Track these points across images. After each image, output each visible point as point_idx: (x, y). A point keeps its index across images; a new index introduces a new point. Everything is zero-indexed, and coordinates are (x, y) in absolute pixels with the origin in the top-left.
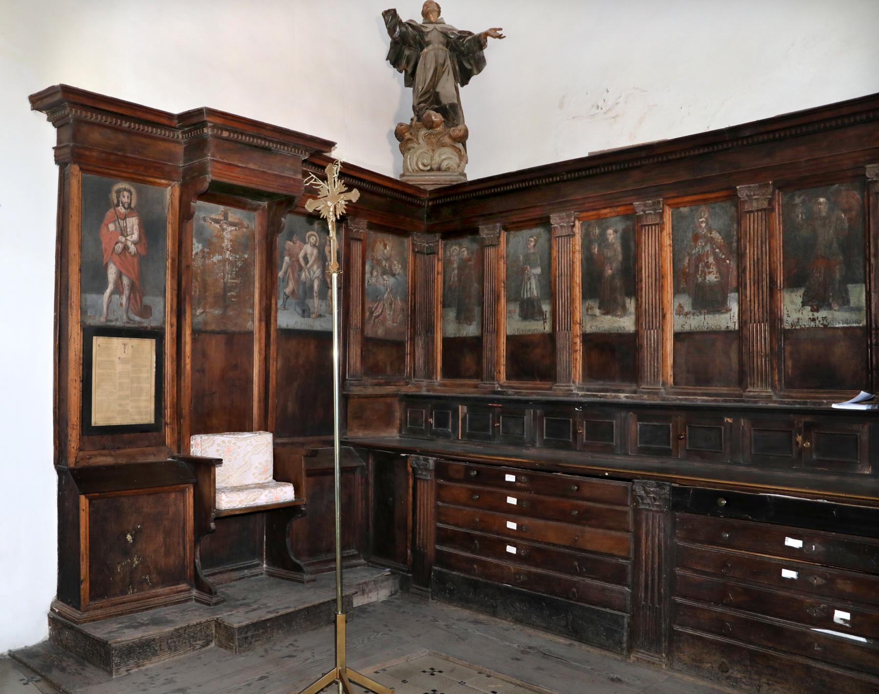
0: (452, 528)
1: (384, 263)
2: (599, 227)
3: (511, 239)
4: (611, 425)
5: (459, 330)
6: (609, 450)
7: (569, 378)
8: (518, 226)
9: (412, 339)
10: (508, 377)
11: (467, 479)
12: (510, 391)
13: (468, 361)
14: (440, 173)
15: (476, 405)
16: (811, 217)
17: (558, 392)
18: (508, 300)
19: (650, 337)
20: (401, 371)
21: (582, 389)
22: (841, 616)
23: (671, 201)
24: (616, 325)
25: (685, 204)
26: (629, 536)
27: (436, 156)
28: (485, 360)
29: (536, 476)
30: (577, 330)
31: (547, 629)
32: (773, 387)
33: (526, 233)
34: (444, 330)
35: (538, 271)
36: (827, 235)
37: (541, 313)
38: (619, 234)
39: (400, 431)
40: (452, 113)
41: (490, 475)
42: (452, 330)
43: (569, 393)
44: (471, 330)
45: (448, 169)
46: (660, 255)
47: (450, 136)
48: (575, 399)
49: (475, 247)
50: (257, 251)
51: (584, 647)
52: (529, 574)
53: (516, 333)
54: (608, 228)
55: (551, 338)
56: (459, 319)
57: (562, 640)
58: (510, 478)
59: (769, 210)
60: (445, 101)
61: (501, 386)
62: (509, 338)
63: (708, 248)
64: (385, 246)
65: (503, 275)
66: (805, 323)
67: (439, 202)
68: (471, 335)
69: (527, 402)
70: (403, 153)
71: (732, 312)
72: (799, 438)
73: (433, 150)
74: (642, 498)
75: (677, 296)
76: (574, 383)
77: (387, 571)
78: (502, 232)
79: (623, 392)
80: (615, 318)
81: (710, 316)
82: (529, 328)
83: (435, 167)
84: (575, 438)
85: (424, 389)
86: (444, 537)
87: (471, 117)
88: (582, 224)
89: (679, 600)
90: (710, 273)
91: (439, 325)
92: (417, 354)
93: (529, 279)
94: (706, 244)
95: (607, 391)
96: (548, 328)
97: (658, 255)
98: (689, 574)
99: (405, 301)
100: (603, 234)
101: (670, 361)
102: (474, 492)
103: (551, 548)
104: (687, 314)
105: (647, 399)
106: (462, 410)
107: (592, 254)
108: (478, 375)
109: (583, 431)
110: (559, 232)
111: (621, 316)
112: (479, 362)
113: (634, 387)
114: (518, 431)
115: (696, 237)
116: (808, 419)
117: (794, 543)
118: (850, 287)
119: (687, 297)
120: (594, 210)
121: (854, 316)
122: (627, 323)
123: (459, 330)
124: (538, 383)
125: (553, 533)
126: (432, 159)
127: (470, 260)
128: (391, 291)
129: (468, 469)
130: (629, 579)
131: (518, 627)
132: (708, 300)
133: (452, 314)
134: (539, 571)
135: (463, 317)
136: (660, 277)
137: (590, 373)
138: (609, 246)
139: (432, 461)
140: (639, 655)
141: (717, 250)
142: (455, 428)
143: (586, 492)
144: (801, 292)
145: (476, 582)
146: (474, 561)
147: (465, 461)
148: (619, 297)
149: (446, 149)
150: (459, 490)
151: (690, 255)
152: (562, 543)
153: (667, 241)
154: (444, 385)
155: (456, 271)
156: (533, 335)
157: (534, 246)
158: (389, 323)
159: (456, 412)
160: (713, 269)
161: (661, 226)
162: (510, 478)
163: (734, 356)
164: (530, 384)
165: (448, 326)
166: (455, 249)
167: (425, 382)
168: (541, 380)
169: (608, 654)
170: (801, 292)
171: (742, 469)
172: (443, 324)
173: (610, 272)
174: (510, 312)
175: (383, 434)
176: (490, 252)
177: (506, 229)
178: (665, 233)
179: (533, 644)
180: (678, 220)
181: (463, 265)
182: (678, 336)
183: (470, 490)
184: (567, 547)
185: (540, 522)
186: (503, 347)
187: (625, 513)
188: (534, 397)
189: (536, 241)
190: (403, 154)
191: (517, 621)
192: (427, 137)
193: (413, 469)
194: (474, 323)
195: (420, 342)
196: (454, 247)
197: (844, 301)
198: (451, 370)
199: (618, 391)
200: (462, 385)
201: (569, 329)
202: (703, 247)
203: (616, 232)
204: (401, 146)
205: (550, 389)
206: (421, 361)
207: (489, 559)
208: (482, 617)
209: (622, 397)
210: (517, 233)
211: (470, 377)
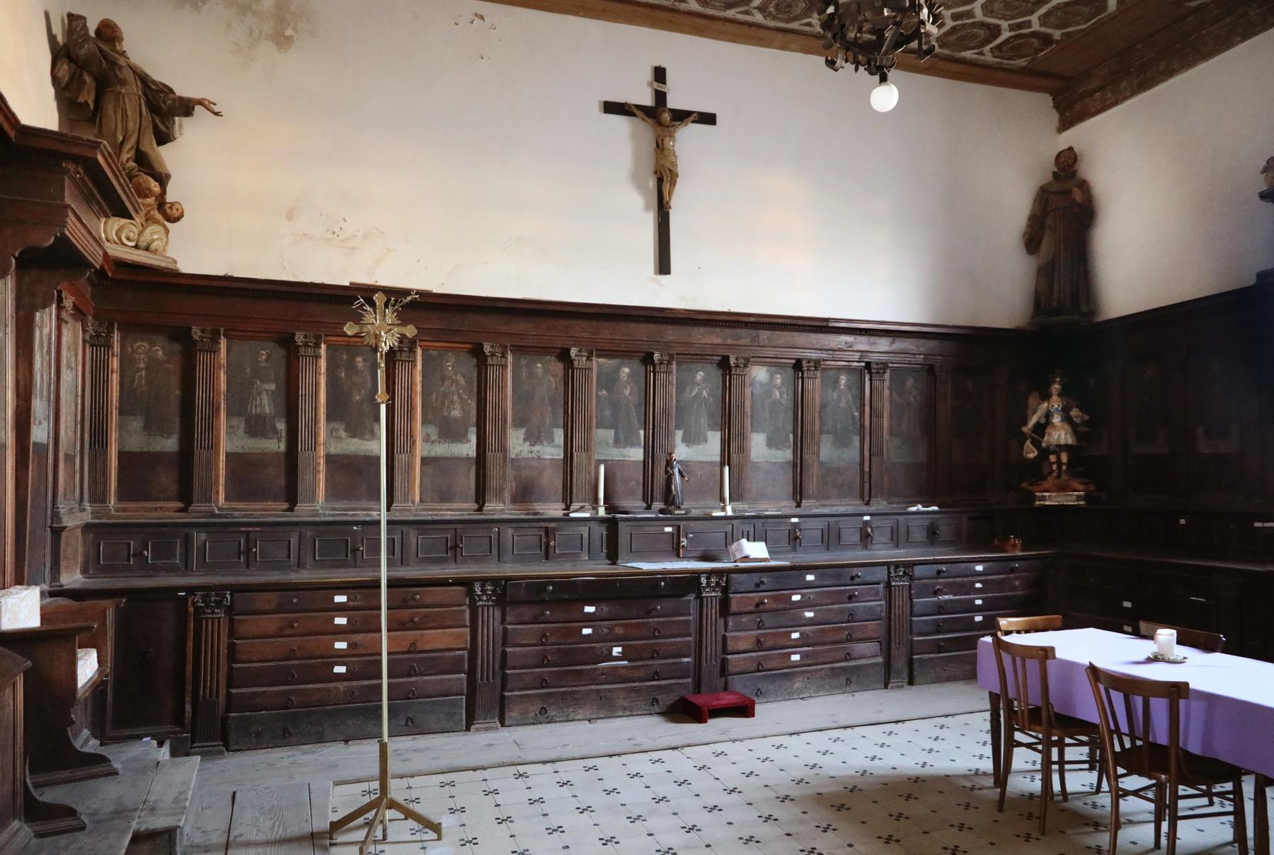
7: (313, 498)
10: (227, 499)
14: (147, 254)
21: (327, 509)
22: (617, 651)
25: (435, 348)
26: (468, 630)
27: (148, 231)
30: (321, 451)
34: (121, 442)
35: (272, 387)
37: (275, 431)
42: (137, 442)
50: (9, 330)
53: (241, 451)
54: (357, 355)
56: (148, 428)
61: (219, 509)
63: (453, 388)
66: (525, 454)
76: (319, 503)
83: (143, 244)
91: (114, 435)
93: (259, 394)
95: (355, 509)
97: (411, 388)
115: (443, 378)
117: (590, 609)
126: (140, 234)
127: (168, 362)
137: (334, 492)
144: (523, 430)
146: (290, 692)
151: (438, 392)
152: (399, 650)
155: (143, 373)
157: (267, 360)
159: (187, 541)
160: (457, 406)
164: (259, 505)
166: (142, 346)
170: (523, 430)
174: (231, 427)
184: (403, 653)
186: (222, 465)
187: (464, 611)
189: (269, 356)
193: (196, 609)
203: (365, 360)
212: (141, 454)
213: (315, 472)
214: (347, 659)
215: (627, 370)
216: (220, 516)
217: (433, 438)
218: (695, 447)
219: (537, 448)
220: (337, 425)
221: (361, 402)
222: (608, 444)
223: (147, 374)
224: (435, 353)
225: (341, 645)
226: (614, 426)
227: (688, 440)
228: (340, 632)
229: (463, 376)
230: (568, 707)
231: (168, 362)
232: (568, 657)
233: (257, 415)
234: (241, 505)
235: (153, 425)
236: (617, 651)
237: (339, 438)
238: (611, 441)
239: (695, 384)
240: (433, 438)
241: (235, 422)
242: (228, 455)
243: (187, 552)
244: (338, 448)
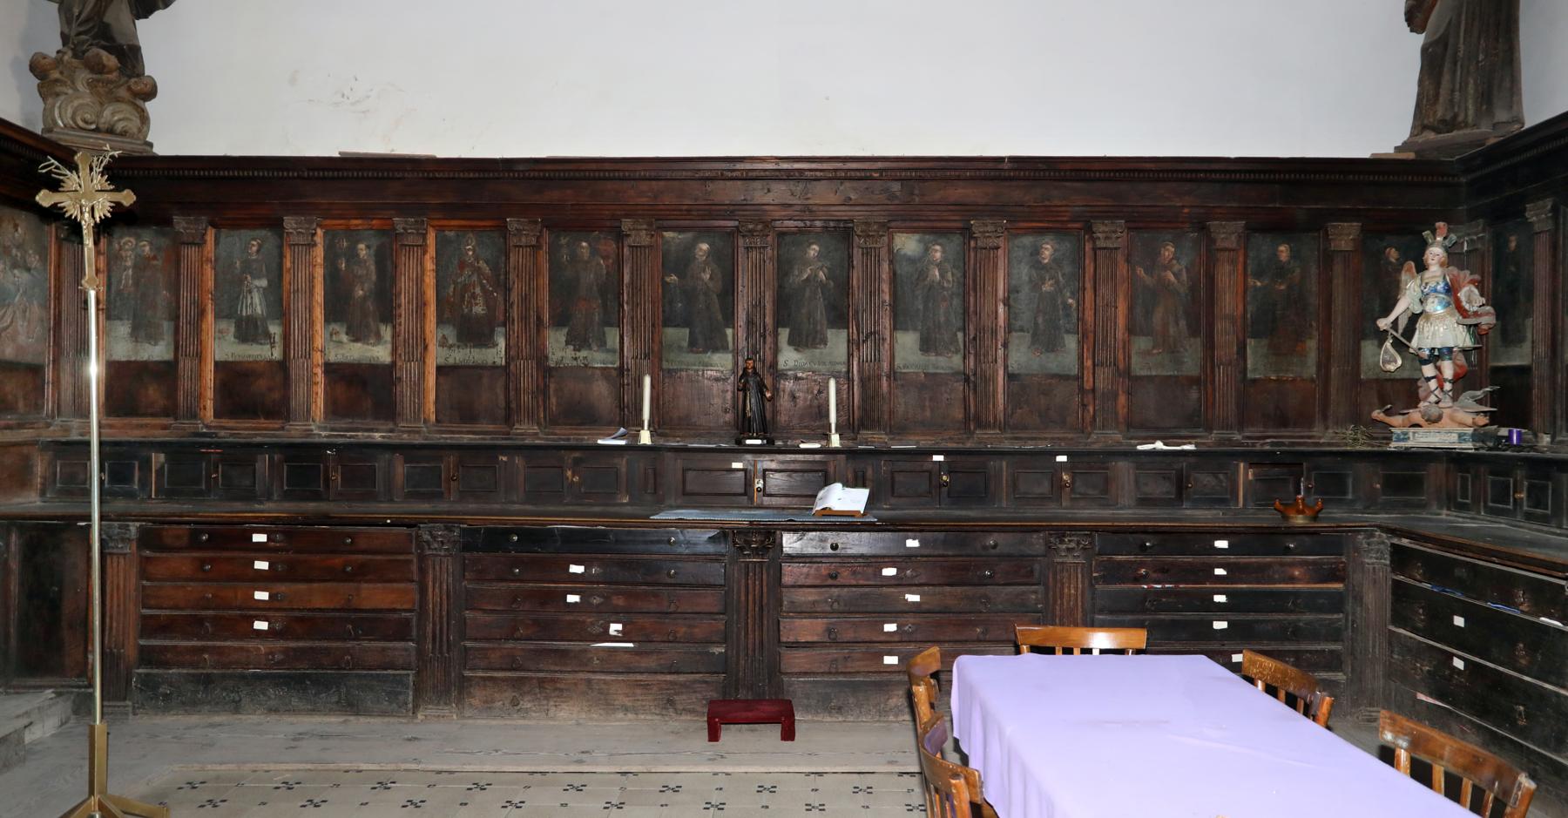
0: (168, 612)
1: (14, 251)
3: (222, 240)
4: (373, 469)
6: (371, 496)
7: (308, 414)
8: (236, 225)
10: (217, 415)
11: (194, 543)
12: (222, 433)
15: (175, 451)
16: (574, 258)
17: (294, 432)
18: (218, 316)
19: (407, 370)
20: (38, 407)
21: (325, 429)
22: (615, 628)
23: (435, 223)
25: (451, 228)
26: (414, 586)
27: (107, 113)
29: (287, 531)
30: (318, 358)
31: (313, 711)
32: (539, 424)
33: (246, 234)
35: (264, 283)
36: (588, 278)
37: (268, 335)
38: (372, 251)
39: (43, 493)
40: (130, 57)
41: (233, 537)
43: (309, 433)
44: (158, 352)
45: (124, 134)
46: (423, 280)
47: (129, 89)
48: (317, 440)
49: (164, 242)
51: (362, 719)
52: (286, 651)
55: (283, 366)
57: (333, 719)
58: (259, 538)
59: (536, 248)
60: (121, 40)
61: (207, 427)
62: (218, 365)
63: (475, 278)
64: (16, 227)
65: (210, 284)
66: (568, 362)
69: (260, 445)
70: (44, 97)
72: (569, 473)
73: (102, 104)
74: (428, 542)
76: (314, 418)
77: (49, 693)
84: (327, 486)
86: (151, 627)
87: (154, 64)
89: (468, 644)
92: (63, 382)
96: (277, 354)
97: (420, 281)
98: (479, 615)
101: (432, 396)
102: (203, 562)
103: (318, 614)
104: (451, 347)
105: (405, 438)
107: (337, 270)
108: (170, 411)
109: (337, 477)
112: (172, 393)
113: (391, 426)
115: (462, 265)
116: (577, 454)
117: (577, 569)
118: (607, 329)
121: (609, 357)
122: (381, 353)
124: (263, 422)
125: (318, 596)
127: (155, 258)
128: (25, 293)
129: (194, 535)
130: (414, 633)
131: (273, 718)
132: (474, 333)
134: (301, 644)
136: (422, 305)
137: (335, 409)
138: (361, 262)
139: (134, 527)
140: (428, 712)
143: (362, 544)
144: (565, 331)
145: (208, 675)
146: (203, 649)
147: (188, 523)
149: (123, 106)
150: (182, 562)
151: (455, 283)
153: (430, 265)
158: (22, 339)
160: (480, 300)
161: (424, 248)
162: (259, 538)
163: (500, 391)
169: (392, 720)
170: (565, 331)
171: (517, 507)
174: (221, 332)
175: (16, 500)
177: (214, 225)
178: (427, 257)
179: (301, 730)
180: (442, 244)
182: (440, 369)
183: (195, 559)
185: (302, 587)
187: (411, 561)
188: (259, 439)
189: (260, 246)
190: (44, 99)
191: (273, 710)
192: (91, 85)
196: (127, 239)
197: (602, 344)
199: (372, 430)
203: (368, 247)
204: (40, 87)
205: (282, 428)
207: (228, 643)
208: (217, 719)
209: (377, 437)
211: (153, 415)
212: (129, 362)
213: (311, 383)
214: (271, 614)
215: (705, 246)
216: (204, 435)
218: (808, 352)
219: (583, 353)
220: (335, 327)
221: (365, 298)
222: (680, 348)
224: (452, 234)
225: (261, 596)
226: (686, 323)
227: (797, 342)
228: (261, 580)
230: (547, 698)
231: (155, 258)
232: (547, 629)
234: (231, 423)
235: (143, 330)
236: (615, 628)
237: (340, 342)
238: (685, 344)
239: (806, 263)
241: (223, 325)
242: (217, 364)
244: (335, 355)
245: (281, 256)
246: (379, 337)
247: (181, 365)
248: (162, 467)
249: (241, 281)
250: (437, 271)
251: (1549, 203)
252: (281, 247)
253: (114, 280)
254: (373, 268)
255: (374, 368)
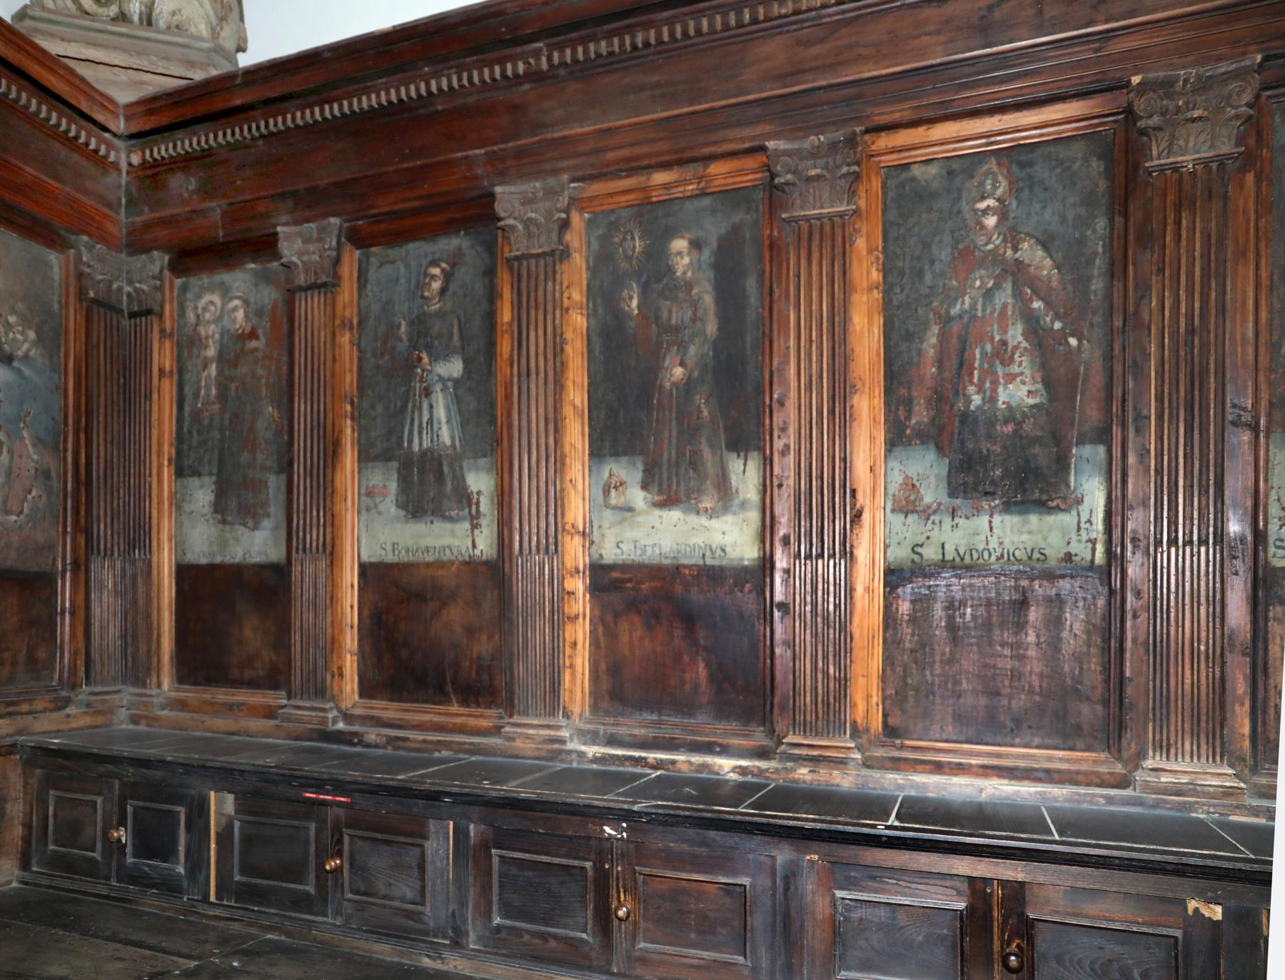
2: (645, 234)
3: (373, 275)
5: (223, 544)
7: (552, 700)
9: (80, 567)
10: (367, 690)
12: (372, 735)
13: (251, 633)
15: (264, 793)
21: (594, 738)
24: (698, 540)
28: (296, 637)
30: (575, 553)
34: (180, 544)
35: (454, 368)
37: (466, 498)
38: (706, 254)
44: (257, 544)
53: (390, 558)
54: (670, 233)
55: (495, 574)
61: (348, 718)
63: (1005, 296)
65: (349, 380)
67: (163, 150)
68: (257, 559)
71: (1084, 510)
75: (898, 451)
76: (568, 732)
78: (348, 247)
79: (725, 751)
80: (693, 519)
81: (1011, 520)
82: (430, 542)
85: (123, 714)
88: (590, 223)
90: (1011, 378)
91: (165, 529)
92: (96, 610)
93: (427, 392)
94: (997, 286)
96: (485, 544)
99: (53, 443)
100: (657, 256)
106: (221, 805)
107: (619, 317)
108: (276, 678)
110: (519, 246)
111: (712, 514)
112: (281, 637)
113: (759, 738)
114: (406, 889)
119: (931, 456)
120: (632, 171)
122: (730, 536)
123: (223, 544)
124: (455, 712)
127: (253, 335)
133: (202, 495)
135: (235, 503)
137: (619, 689)
141: (1037, 304)
142: (197, 863)
148: (707, 453)
154: (182, 705)
155: (213, 370)
156: (440, 564)
157: (443, 291)
159: (199, 809)
160: (1023, 364)
165: (188, 529)
167: (127, 694)
168: (465, 702)
172: (180, 525)
173: (678, 372)
176: (311, 308)
177: (359, 239)
181: (235, 349)
189: (448, 276)
194: (266, 523)
195: (106, 574)
196: (207, 298)
198: (203, 660)
199: (708, 748)
200: (230, 708)
201: (553, 548)
202: (988, 294)
203: (696, 245)
205: (496, 731)
206: (114, 631)
210: (392, 253)
211: (254, 684)
212: (212, 567)
213: (559, 620)
216: (338, 737)
217: (928, 498)
220: (619, 469)
221: (688, 387)
223: (220, 371)
229: (1046, 244)
231: (253, 335)
233: (424, 454)
240: (928, 498)
242: (365, 569)
243: (804, 760)
245: (492, 295)
246: (725, 491)
247: (296, 569)
248: (230, 826)
249: (409, 366)
250: (887, 292)
251: (972, 408)
252: (490, 273)
253: (188, 390)
254: (709, 300)
255: (713, 575)
